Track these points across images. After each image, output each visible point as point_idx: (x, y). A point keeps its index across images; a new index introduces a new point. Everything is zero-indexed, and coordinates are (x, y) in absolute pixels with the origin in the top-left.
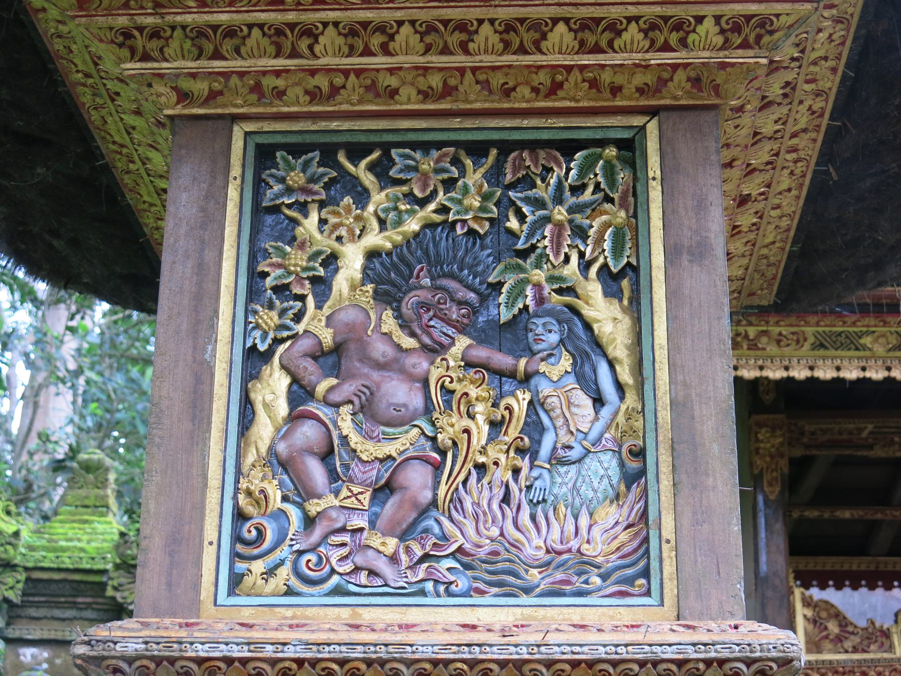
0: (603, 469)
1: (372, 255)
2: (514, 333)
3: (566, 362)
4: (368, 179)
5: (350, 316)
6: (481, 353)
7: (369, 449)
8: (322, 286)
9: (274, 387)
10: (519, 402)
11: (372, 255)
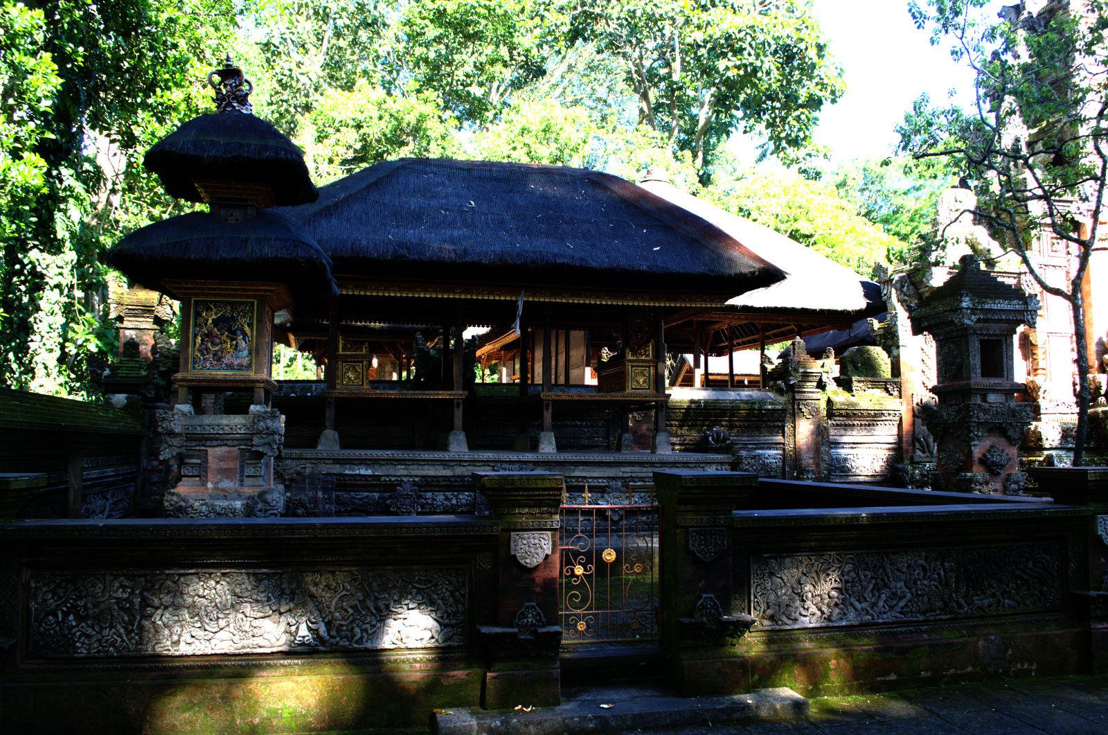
0: (246, 352)
2: (234, 333)
7: (212, 349)
8: (206, 324)
9: (199, 340)
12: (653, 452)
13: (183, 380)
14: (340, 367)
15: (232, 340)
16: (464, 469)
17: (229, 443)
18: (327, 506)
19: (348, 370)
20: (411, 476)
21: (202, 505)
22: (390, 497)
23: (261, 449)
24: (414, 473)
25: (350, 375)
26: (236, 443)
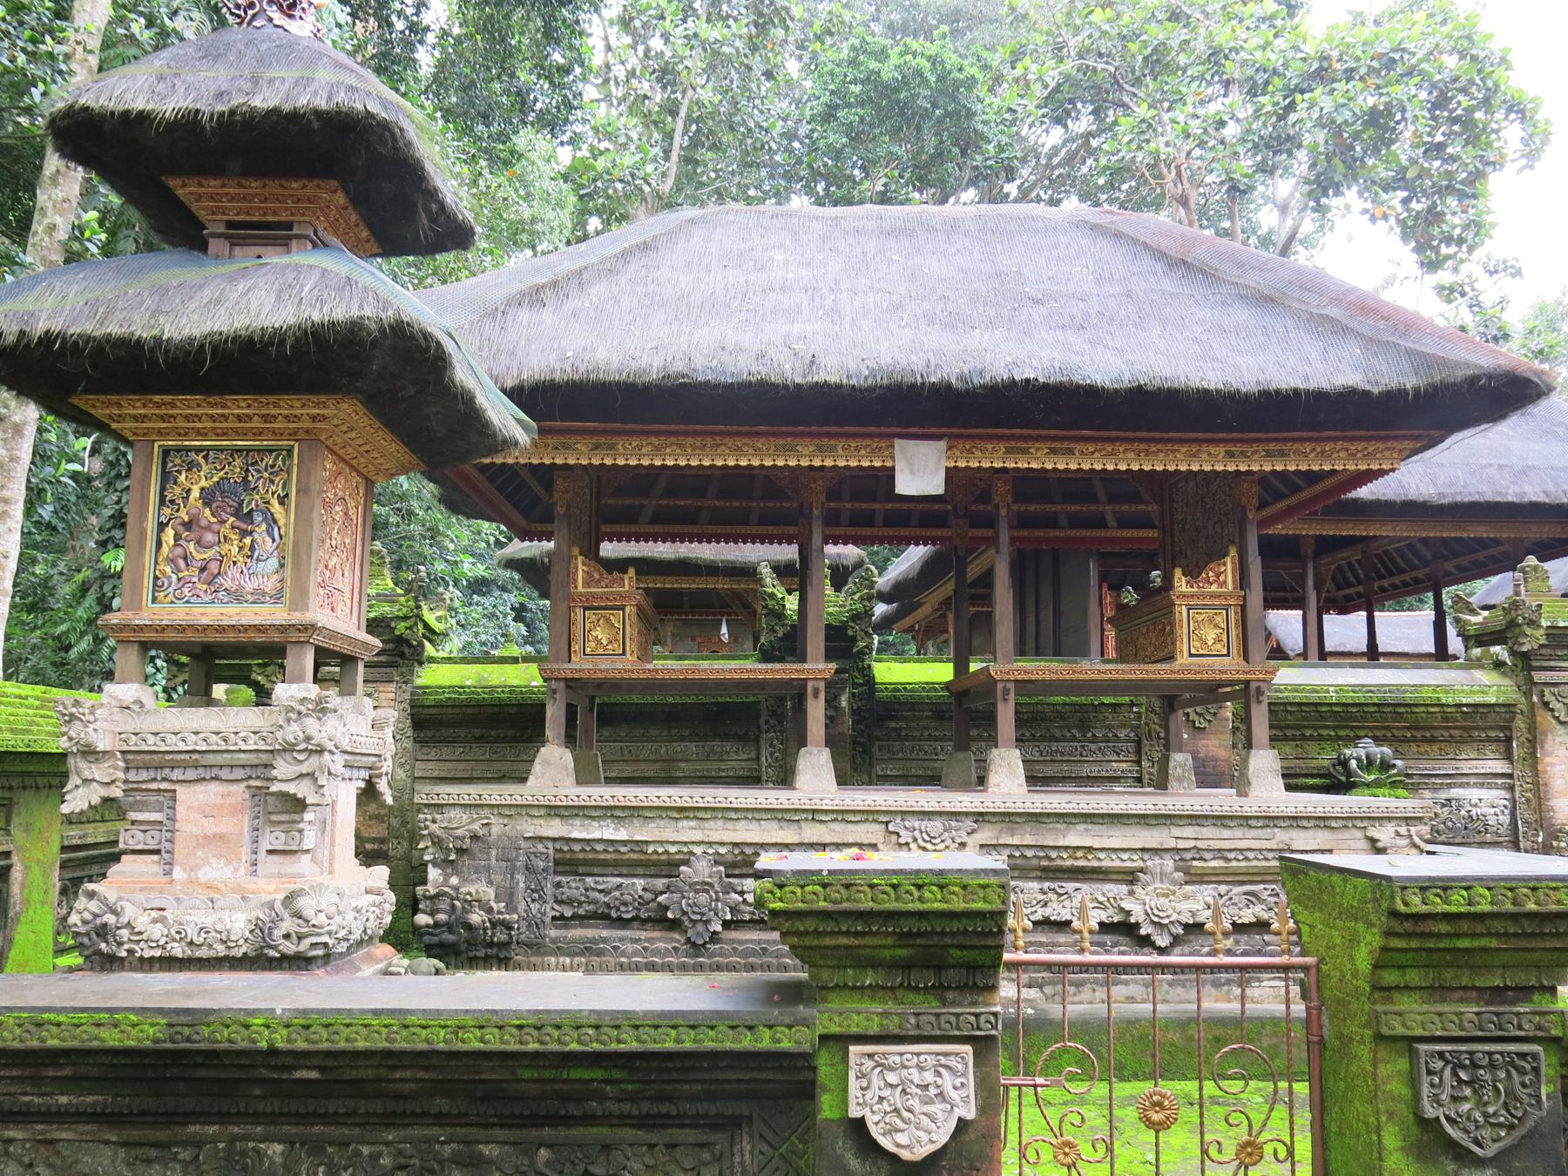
0: (273, 563)
1: (202, 489)
3: (264, 527)
4: (202, 461)
5: (194, 511)
6: (237, 524)
7: (198, 556)
9: (169, 534)
10: (248, 541)
11: (202, 489)
12: (1242, 793)
13: (123, 627)
14: (580, 618)
15: (244, 533)
16: (822, 828)
17: (224, 774)
18: (535, 907)
19: (596, 624)
20: (710, 844)
21: (155, 921)
22: (668, 889)
23: (291, 788)
24: (715, 837)
25: (600, 633)
26: (239, 774)
